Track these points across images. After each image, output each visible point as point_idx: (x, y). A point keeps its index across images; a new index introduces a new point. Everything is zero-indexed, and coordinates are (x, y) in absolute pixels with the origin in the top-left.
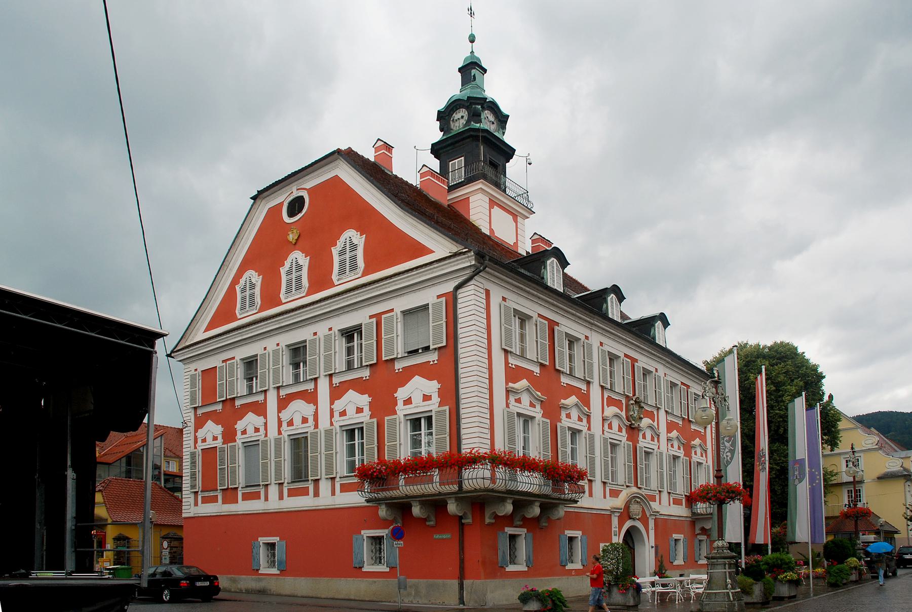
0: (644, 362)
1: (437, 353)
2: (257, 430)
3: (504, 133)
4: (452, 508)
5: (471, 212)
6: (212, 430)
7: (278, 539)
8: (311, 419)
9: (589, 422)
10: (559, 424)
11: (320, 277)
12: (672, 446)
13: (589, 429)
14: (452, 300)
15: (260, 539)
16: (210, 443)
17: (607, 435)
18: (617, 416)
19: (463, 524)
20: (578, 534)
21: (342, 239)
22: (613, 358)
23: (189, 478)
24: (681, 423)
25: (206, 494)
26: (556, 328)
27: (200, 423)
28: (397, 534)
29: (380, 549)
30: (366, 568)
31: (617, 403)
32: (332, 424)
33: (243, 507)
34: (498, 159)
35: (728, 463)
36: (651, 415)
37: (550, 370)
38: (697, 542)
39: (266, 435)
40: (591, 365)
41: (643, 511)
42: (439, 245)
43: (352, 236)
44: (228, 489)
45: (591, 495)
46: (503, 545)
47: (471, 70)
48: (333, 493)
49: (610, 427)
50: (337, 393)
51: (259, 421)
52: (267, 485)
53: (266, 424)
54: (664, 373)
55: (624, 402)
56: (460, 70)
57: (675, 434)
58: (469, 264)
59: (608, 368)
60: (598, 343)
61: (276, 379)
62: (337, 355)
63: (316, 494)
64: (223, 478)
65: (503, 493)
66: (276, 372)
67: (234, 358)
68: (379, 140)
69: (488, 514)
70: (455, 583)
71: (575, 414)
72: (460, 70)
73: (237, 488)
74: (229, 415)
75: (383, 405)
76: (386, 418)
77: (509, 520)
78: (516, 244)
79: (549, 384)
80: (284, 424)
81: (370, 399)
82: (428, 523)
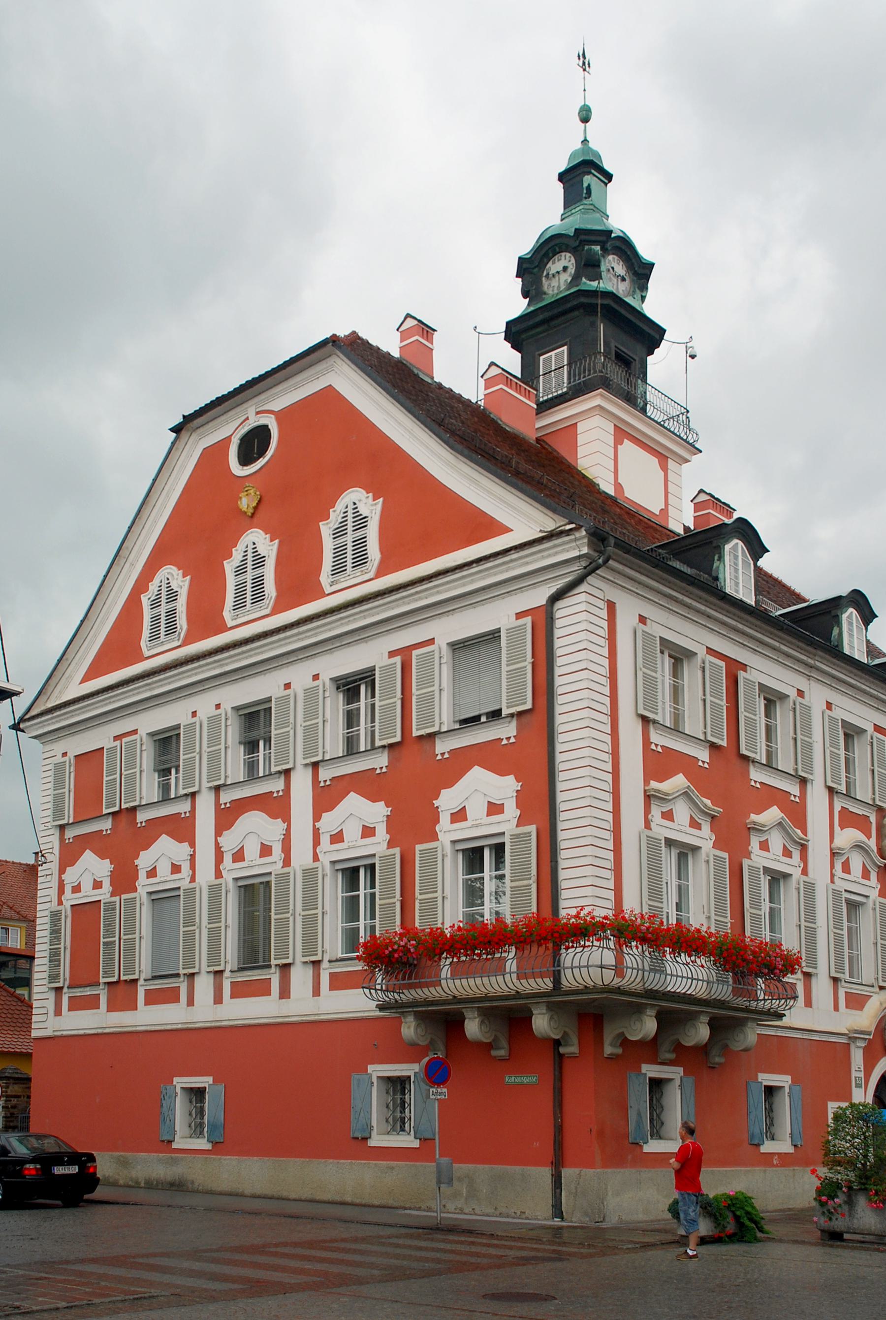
1: (514, 723)
3: (643, 298)
5: (581, 452)
6: (93, 867)
7: (210, 1080)
8: (277, 849)
9: (804, 857)
10: (746, 862)
13: (805, 872)
14: (544, 622)
16: (88, 894)
17: (841, 885)
18: (859, 847)
19: (561, 1056)
21: (340, 506)
22: (851, 733)
25: (78, 992)
26: (742, 675)
28: (436, 1074)
29: (403, 1102)
30: (377, 1141)
31: (860, 822)
32: (316, 858)
33: (147, 1017)
34: (631, 349)
37: (730, 756)
39: (193, 879)
42: (521, 517)
43: (359, 500)
44: (118, 982)
45: (808, 1003)
47: (583, 176)
48: (316, 992)
49: (846, 868)
50: (326, 798)
51: (179, 851)
52: (193, 975)
53: (193, 857)
55: (873, 819)
56: (562, 177)
58: (576, 553)
59: (842, 752)
62: (328, 726)
63: (285, 993)
64: (109, 961)
66: (214, 758)
67: (135, 732)
68: (408, 316)
70: (545, 1173)
71: (776, 841)
72: (562, 177)
73: (136, 981)
74: (124, 839)
75: (412, 823)
76: (418, 847)
77: (649, 1050)
78: (664, 512)
79: (727, 784)
80: (228, 858)
81: (387, 811)
82: (494, 1053)
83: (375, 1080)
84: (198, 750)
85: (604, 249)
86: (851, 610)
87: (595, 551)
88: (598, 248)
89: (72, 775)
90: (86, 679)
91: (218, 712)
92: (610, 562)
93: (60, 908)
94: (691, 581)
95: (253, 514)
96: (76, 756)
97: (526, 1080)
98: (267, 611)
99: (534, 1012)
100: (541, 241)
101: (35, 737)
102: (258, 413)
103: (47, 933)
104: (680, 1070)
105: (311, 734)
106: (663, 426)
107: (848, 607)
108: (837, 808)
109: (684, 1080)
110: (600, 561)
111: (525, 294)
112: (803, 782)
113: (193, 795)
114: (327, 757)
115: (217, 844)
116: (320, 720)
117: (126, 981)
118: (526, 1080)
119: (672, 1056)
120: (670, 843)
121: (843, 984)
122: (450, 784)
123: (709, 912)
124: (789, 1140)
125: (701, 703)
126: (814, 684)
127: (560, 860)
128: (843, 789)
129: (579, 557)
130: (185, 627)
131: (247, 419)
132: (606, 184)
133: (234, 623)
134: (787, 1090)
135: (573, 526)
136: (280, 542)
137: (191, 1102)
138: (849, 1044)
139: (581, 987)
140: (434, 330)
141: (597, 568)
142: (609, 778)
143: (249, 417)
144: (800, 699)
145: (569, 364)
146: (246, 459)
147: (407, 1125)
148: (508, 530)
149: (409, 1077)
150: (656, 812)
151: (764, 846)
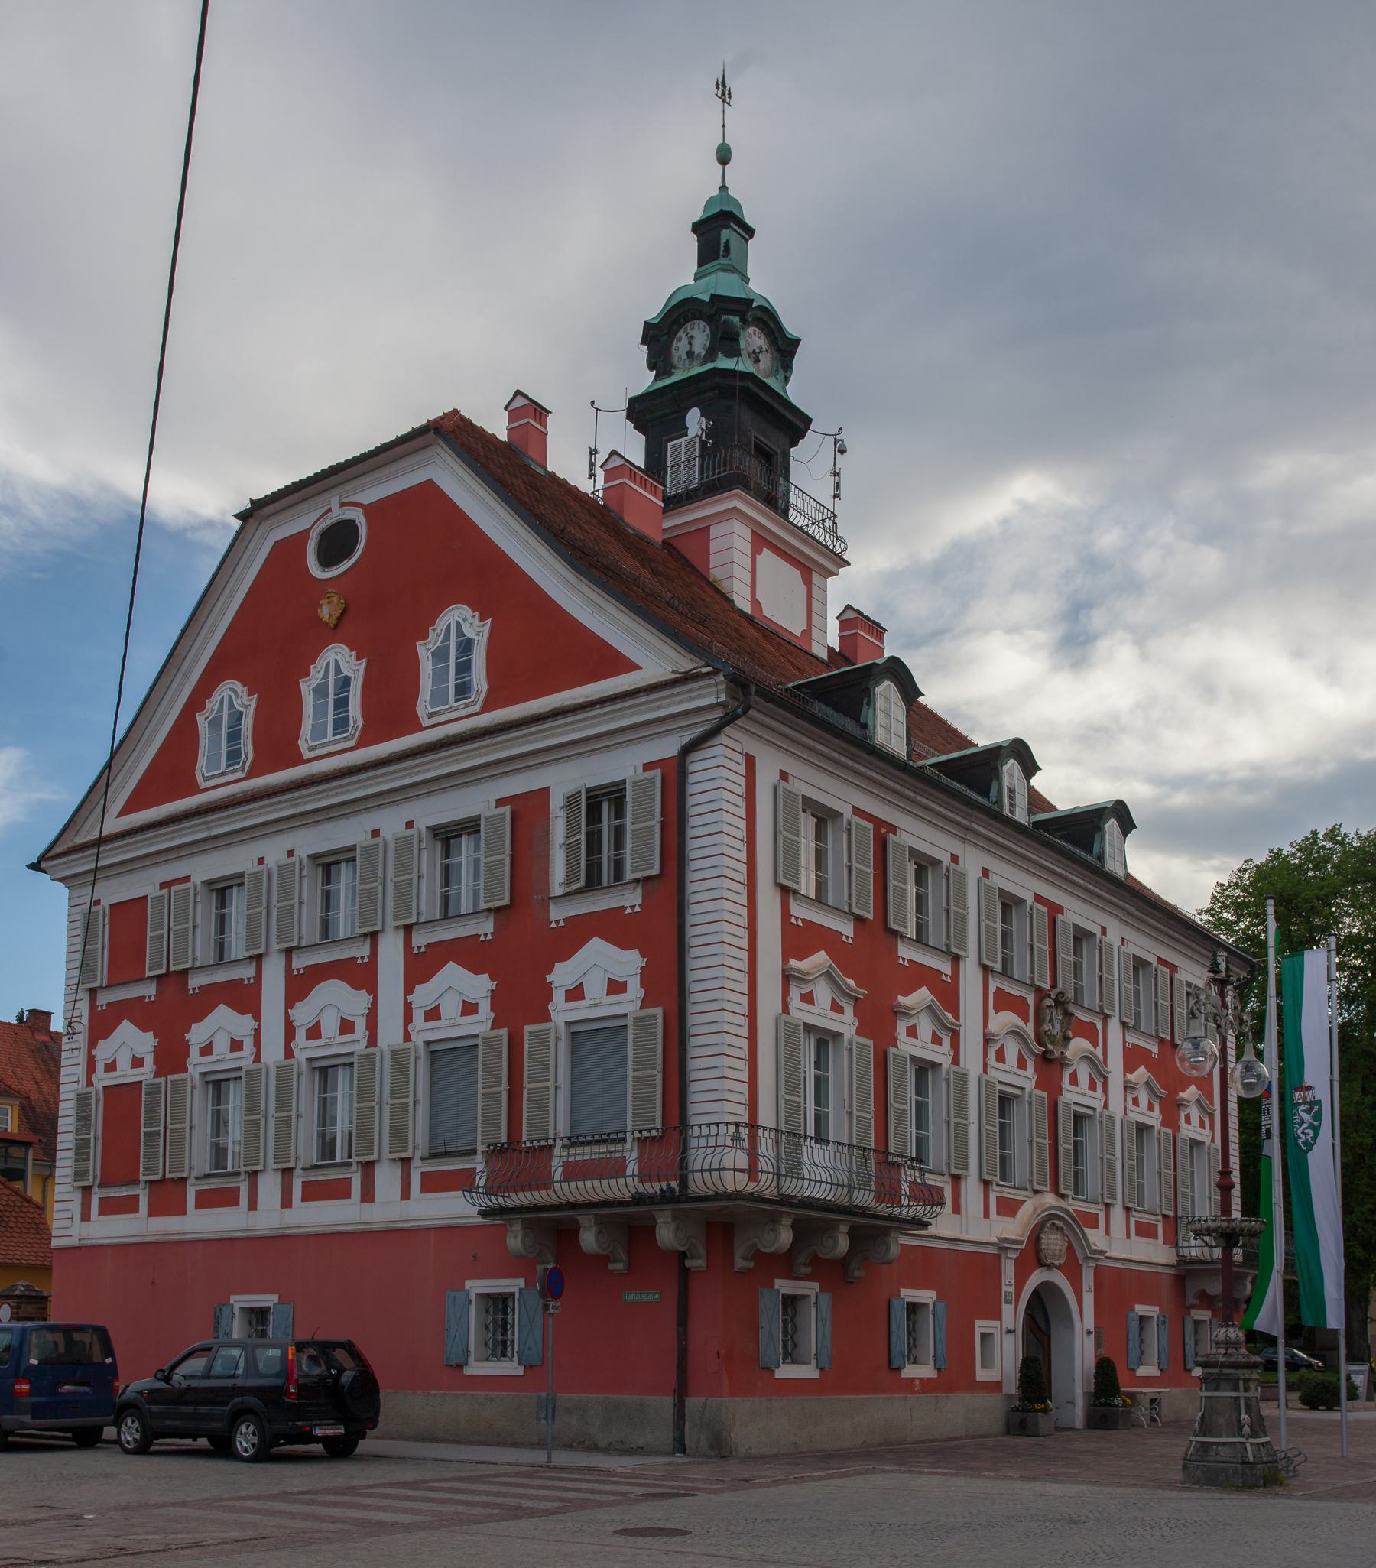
0: (1077, 912)
1: (639, 890)
2: (236, 1046)
3: (787, 380)
4: (666, 1234)
5: (714, 560)
6: (131, 1042)
7: (275, 1298)
8: (361, 1025)
9: (955, 1045)
10: (892, 1050)
11: (390, 705)
12: (1136, 1102)
13: (955, 1061)
14: (674, 777)
15: (233, 1299)
16: (125, 1074)
17: (995, 1075)
18: (1015, 1033)
19: (687, 1269)
20: (927, 1296)
21: (441, 624)
22: (1009, 903)
23: (70, 1154)
24: (1155, 1049)
25: (113, 1193)
26: (891, 837)
27: (101, 1026)
28: (553, 1287)
29: (505, 1322)
30: (476, 1368)
31: (1016, 1005)
32: (407, 1037)
33: (197, 1222)
34: (773, 441)
35: (1310, 1146)
36: (1089, 1032)
37: (878, 930)
38: (1189, 1328)
39: (257, 1058)
40: (963, 919)
41: (1070, 1248)
42: (653, 658)
43: (460, 620)
44: (163, 1180)
45: (956, 1209)
46: (771, 1323)
47: (720, 231)
48: (405, 1194)
49: (1001, 1057)
50: (420, 967)
51: (241, 1025)
52: (256, 1173)
53: (257, 1033)
54: (1123, 940)
55: (1031, 1001)
56: (696, 228)
57: (1141, 1074)
58: (712, 700)
59: (999, 926)
60: (980, 868)
61: (285, 932)
62: (424, 882)
63: (368, 1196)
64: (152, 1156)
65: (769, 1201)
66: (286, 915)
67: (187, 879)
68: (518, 393)
69: (739, 1251)
70: (667, 1402)
71: (926, 1027)
72: (696, 228)
73: (184, 1179)
74: (172, 1011)
75: (521, 1002)
76: (528, 1028)
77: (785, 1264)
78: (807, 633)
79: (872, 966)
80: (301, 1035)
81: (492, 985)
82: (611, 1266)
83: (473, 1297)
84: (265, 904)
85: (744, 321)
86: (1012, 761)
87: (733, 698)
88: (736, 319)
89: (107, 927)
90: (126, 811)
91: (291, 860)
92: (751, 712)
93: (90, 1089)
94: (840, 734)
95: (336, 626)
96: (111, 906)
97: (647, 1297)
98: (352, 743)
99: (660, 1221)
100: (673, 303)
101: (60, 880)
102: (342, 505)
103: (72, 1120)
104: (816, 1286)
105: (404, 893)
106: (807, 533)
107: (1008, 757)
108: (992, 989)
109: (821, 1296)
110: (740, 710)
111: (652, 365)
112: (956, 959)
113: (259, 958)
114: (423, 919)
115: (287, 1017)
116: (414, 875)
117: (172, 1179)
118: (647, 1297)
119: (808, 1270)
120: (809, 1028)
121: (995, 1187)
122: (566, 956)
123: (850, 1106)
124: (932, 1363)
125: (845, 871)
126: (968, 847)
127: (689, 1049)
128: (998, 967)
129: (718, 705)
130: (251, 756)
131: (330, 510)
132: (747, 241)
133: (312, 754)
134: (931, 1307)
135: (709, 669)
136: (368, 663)
137: (251, 1324)
138: (999, 1256)
139: (711, 1193)
140: (549, 412)
141: (737, 717)
142: (744, 955)
143: (334, 509)
144: (953, 865)
145: (702, 456)
146: (326, 561)
147: (509, 1350)
148: (634, 667)
149: (513, 1294)
150: (795, 994)
151: (912, 1032)
